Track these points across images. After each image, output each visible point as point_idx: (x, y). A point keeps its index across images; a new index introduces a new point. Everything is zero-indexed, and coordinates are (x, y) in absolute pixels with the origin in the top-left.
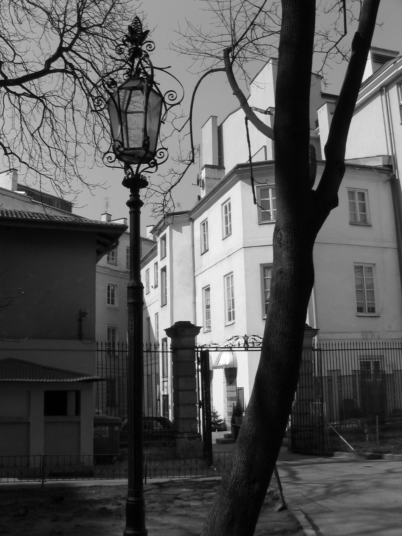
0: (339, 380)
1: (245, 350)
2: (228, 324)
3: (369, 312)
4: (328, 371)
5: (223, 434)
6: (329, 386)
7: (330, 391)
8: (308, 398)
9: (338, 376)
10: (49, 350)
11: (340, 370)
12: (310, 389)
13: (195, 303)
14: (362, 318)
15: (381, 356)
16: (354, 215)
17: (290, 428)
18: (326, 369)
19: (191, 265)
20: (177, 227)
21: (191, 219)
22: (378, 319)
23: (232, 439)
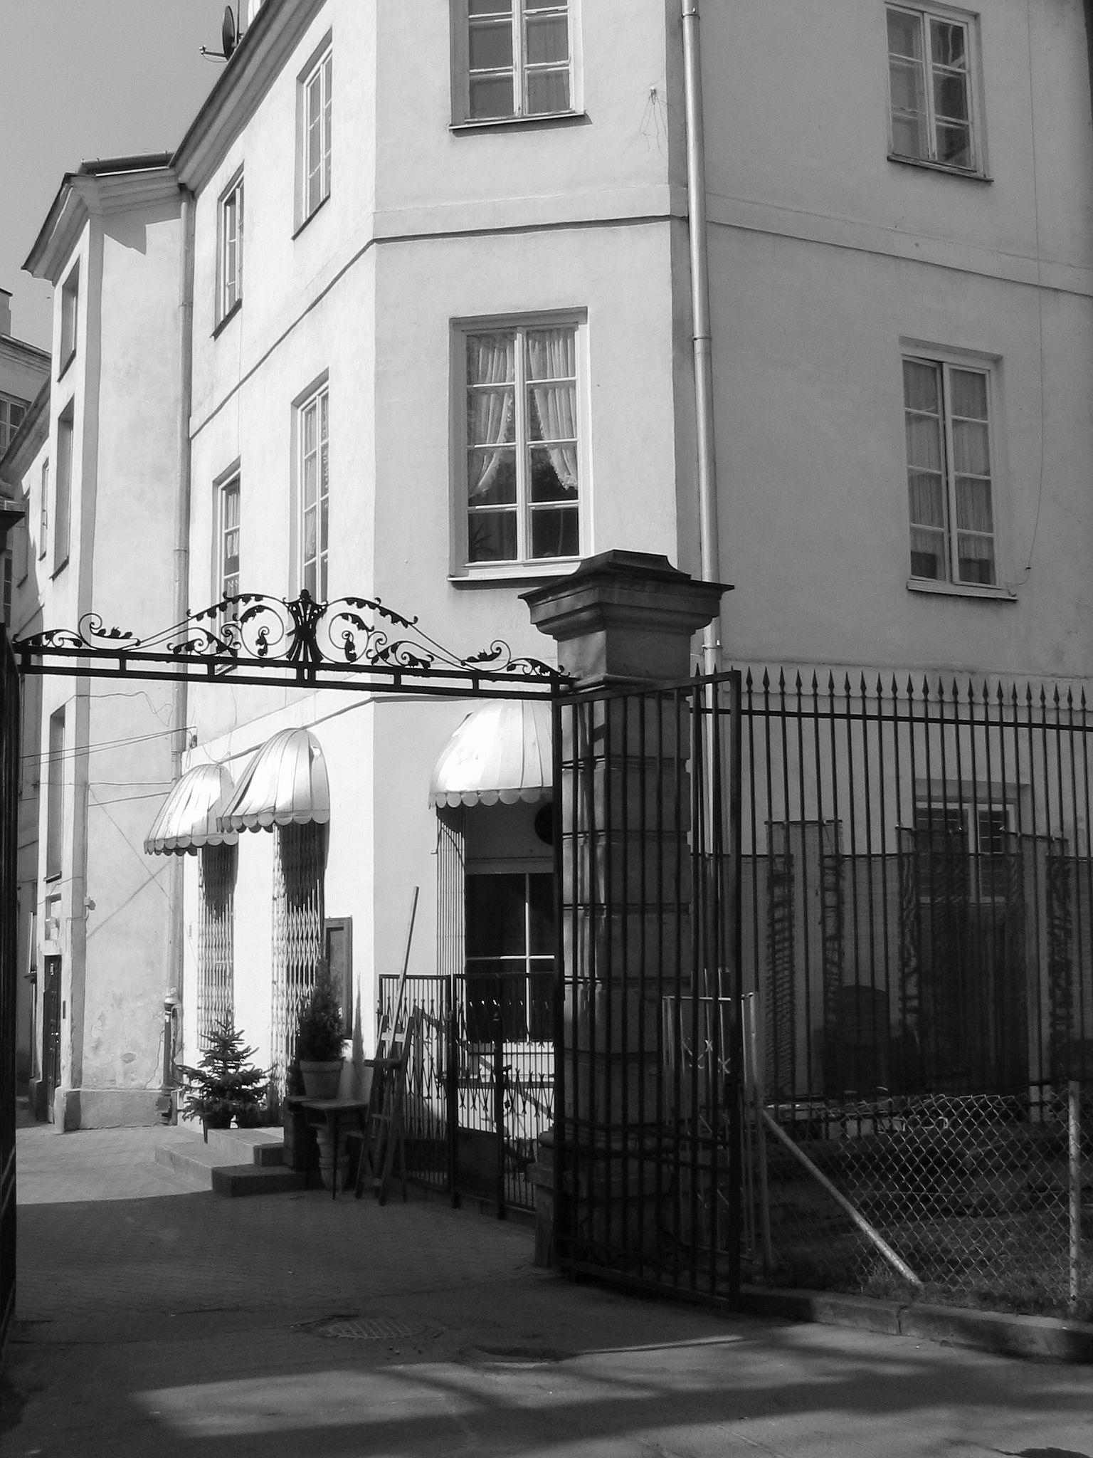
0: (830, 879)
1: (299, 682)
3: (965, 576)
4: (770, 824)
5: (251, 1146)
6: (773, 906)
7: (780, 937)
8: (651, 972)
9: (822, 857)
11: (836, 822)
12: (670, 919)
13: (185, 551)
14: (934, 604)
15: (1019, 787)
16: (909, 126)
17: (551, 1137)
18: (762, 816)
19: (177, 389)
20: (126, 223)
21: (182, 187)
22: (1006, 612)
23: (284, 1171)
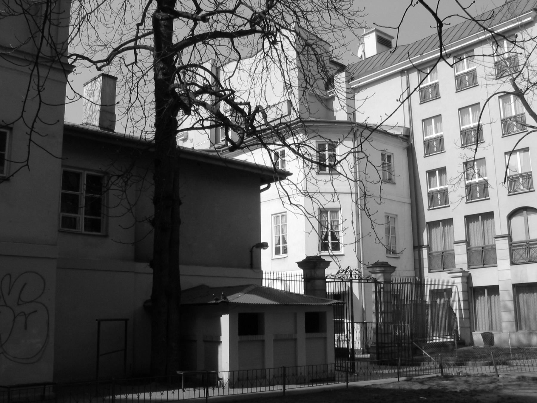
2: (274, 257)
10: (121, 271)
